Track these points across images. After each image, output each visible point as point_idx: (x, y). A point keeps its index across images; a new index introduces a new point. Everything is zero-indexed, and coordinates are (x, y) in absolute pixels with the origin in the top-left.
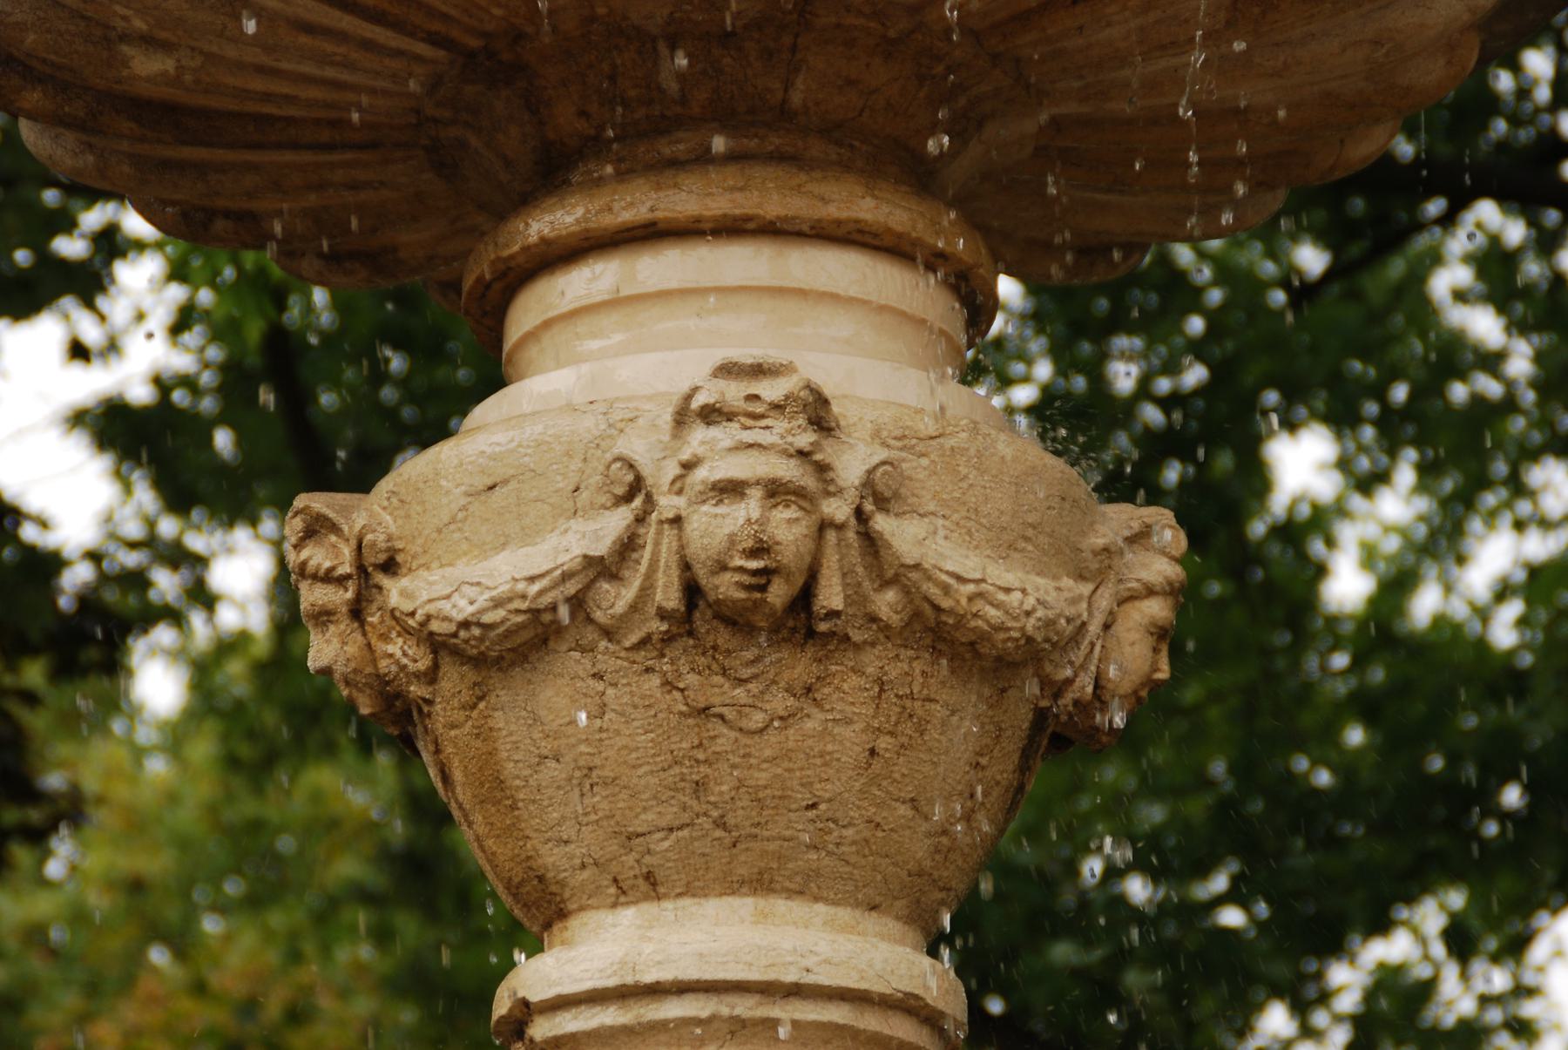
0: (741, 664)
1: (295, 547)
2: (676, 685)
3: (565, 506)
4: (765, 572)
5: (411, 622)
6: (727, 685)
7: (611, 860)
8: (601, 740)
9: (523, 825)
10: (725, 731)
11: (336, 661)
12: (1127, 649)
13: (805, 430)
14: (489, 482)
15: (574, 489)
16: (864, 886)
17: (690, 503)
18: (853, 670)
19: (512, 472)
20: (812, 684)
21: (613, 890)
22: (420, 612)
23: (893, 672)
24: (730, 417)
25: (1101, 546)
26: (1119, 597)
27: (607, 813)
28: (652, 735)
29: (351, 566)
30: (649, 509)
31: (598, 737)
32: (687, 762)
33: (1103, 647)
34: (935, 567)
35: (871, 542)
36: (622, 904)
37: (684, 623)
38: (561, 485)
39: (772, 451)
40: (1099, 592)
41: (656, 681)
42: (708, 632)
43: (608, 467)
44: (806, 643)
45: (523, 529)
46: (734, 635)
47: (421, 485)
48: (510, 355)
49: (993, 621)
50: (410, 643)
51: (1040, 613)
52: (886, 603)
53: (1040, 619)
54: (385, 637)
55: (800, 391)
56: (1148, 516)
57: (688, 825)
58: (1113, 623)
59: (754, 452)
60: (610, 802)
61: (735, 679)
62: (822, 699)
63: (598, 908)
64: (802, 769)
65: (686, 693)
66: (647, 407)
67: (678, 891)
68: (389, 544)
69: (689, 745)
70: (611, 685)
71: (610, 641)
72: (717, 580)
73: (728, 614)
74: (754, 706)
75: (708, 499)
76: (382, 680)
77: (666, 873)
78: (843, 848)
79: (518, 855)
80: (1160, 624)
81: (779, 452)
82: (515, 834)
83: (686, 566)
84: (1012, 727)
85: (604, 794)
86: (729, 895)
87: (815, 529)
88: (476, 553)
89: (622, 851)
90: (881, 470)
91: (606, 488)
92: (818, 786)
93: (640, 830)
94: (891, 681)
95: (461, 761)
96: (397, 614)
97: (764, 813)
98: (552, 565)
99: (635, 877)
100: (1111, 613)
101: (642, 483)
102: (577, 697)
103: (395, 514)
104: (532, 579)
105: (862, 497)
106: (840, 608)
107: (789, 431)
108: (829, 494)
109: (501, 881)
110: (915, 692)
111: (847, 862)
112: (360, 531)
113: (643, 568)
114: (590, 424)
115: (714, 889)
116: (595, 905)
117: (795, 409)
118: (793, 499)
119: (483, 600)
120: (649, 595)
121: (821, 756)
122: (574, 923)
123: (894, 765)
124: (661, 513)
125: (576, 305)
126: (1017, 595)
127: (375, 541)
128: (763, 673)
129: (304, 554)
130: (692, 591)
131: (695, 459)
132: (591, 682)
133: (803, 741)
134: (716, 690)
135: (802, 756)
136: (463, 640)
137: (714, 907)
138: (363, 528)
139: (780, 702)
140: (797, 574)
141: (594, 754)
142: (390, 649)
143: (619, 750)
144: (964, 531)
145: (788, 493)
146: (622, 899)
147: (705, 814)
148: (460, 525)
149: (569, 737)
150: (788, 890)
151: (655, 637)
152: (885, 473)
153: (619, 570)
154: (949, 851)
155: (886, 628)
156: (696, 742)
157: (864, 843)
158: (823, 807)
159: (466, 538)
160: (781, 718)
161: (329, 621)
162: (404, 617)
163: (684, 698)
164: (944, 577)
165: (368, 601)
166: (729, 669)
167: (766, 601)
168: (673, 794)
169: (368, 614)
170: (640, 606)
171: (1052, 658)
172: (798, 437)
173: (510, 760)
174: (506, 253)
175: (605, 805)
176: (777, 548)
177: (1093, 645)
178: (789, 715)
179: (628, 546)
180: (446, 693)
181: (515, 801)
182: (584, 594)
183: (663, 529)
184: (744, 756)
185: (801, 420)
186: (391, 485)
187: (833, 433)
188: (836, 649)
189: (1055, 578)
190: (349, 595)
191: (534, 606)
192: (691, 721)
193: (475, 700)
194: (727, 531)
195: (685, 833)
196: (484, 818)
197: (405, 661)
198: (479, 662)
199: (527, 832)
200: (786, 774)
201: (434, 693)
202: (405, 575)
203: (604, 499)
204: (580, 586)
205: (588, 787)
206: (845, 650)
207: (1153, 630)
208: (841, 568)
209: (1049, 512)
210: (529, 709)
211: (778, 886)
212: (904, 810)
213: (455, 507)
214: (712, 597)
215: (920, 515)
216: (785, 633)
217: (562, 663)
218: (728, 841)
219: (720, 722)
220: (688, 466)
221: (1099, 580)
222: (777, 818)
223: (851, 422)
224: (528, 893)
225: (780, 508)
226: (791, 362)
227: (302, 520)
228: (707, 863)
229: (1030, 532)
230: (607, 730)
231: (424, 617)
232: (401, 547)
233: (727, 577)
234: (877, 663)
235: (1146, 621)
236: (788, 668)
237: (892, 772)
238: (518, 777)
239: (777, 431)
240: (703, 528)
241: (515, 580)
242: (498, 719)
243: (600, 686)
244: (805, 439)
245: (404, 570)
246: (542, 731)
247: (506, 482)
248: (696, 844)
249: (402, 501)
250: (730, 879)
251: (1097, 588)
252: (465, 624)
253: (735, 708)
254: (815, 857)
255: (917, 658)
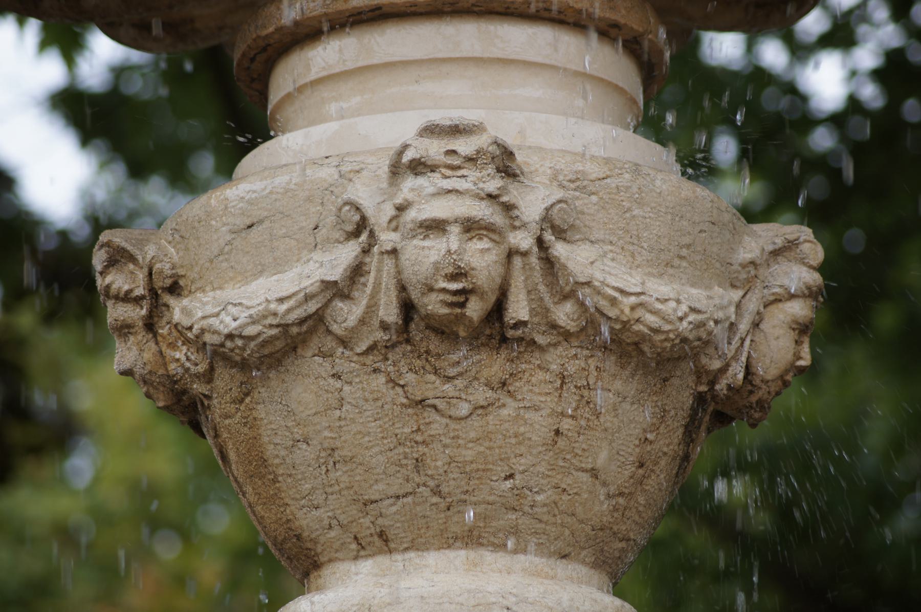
0: (449, 365)
1: (101, 273)
2: (398, 382)
3: (308, 241)
4: (464, 292)
5: (189, 335)
6: (438, 382)
7: (352, 522)
8: (340, 427)
9: (283, 494)
10: (438, 418)
11: (136, 365)
12: (773, 343)
13: (493, 178)
14: (248, 223)
15: (314, 227)
16: (555, 539)
17: (404, 238)
18: (539, 366)
19: (266, 214)
20: (506, 379)
21: (354, 546)
22: (196, 327)
23: (572, 368)
24: (433, 168)
25: (748, 260)
26: (764, 300)
27: (348, 484)
28: (381, 422)
29: (144, 289)
30: (373, 243)
31: (338, 424)
32: (408, 443)
33: (752, 341)
34: (602, 283)
35: (549, 263)
36: (362, 557)
37: (403, 333)
38: (304, 224)
39: (467, 196)
40: (748, 296)
41: (382, 379)
42: (422, 340)
43: (340, 210)
44: (500, 347)
45: (275, 259)
46: (443, 341)
47: (196, 224)
48: (272, 113)
49: (652, 326)
50: (192, 350)
51: (692, 317)
52: (564, 315)
53: (690, 323)
54: (173, 346)
55: (488, 148)
56: (792, 233)
57: (411, 493)
58: (760, 321)
59: (453, 197)
60: (349, 476)
61: (444, 376)
62: (514, 391)
63: (343, 560)
64: (501, 447)
65: (406, 388)
66: (370, 161)
67: (405, 545)
68: (174, 271)
69: (409, 430)
70: (347, 383)
71: (345, 348)
72: (426, 300)
73: (436, 325)
74: (460, 398)
75: (417, 235)
76: (172, 380)
77: (396, 532)
78: (536, 509)
79: (280, 519)
80: (801, 321)
81: (472, 196)
82: (277, 502)
83: (402, 288)
84: (674, 408)
85: (344, 469)
86: (445, 549)
87: (504, 255)
88: (240, 279)
89: (361, 515)
90: (560, 205)
91: (338, 227)
92: (514, 460)
93: (373, 498)
94: (571, 375)
95: (234, 445)
96: (180, 328)
97: (471, 483)
98: (297, 288)
99: (371, 535)
100: (758, 313)
101: (367, 222)
102: (321, 393)
103: (178, 247)
104: (281, 300)
105: (542, 229)
106: (526, 319)
107: (480, 179)
108: (515, 228)
109: (269, 538)
110: (590, 383)
111: (540, 521)
112: (150, 261)
113: (369, 290)
114: (327, 173)
115: (433, 544)
116: (341, 558)
117: (485, 161)
118: (485, 233)
119: (242, 320)
120: (374, 311)
121: (516, 437)
122: (326, 571)
123: (575, 442)
124: (381, 246)
125: (324, 73)
126: (673, 304)
127: (162, 269)
128: (466, 371)
129: (108, 279)
130: (408, 308)
131: (406, 203)
132: (331, 381)
133: (501, 425)
134: (430, 386)
135: (500, 437)
136: (229, 349)
137: (433, 558)
138: (153, 258)
139: (481, 395)
140: (490, 293)
141: (335, 438)
142: (178, 355)
143: (354, 434)
144: (627, 254)
145: (480, 229)
146: (362, 553)
147: (425, 485)
148: (227, 256)
149: (315, 424)
150: (493, 544)
151: (379, 345)
152: (561, 210)
153: (350, 291)
154: (625, 509)
155: (567, 335)
156: (415, 428)
157: (553, 505)
158: (518, 477)
159: (232, 267)
160: (482, 407)
161: (129, 333)
162: (184, 331)
163: (405, 392)
164: (610, 292)
165: (159, 316)
166: (439, 369)
167: (465, 315)
168: (398, 469)
169: (159, 327)
170: (367, 320)
171: (707, 352)
172: (488, 183)
173: (270, 443)
174: (265, 32)
175: (345, 478)
176: (472, 272)
177: (743, 340)
178: (489, 405)
179: (357, 271)
180: (221, 390)
181: (276, 476)
182: (323, 311)
183: (383, 259)
184: (453, 438)
185: (491, 170)
186: (174, 225)
187: (517, 178)
188: (525, 351)
189: (708, 287)
190: (144, 312)
191: (283, 322)
192: (410, 411)
193: (243, 396)
194: (432, 259)
195: (409, 499)
196: (254, 489)
197: (188, 364)
198: (244, 366)
199: (287, 500)
200: (488, 452)
201: (211, 390)
202: (188, 296)
203: (337, 235)
204: (320, 305)
205: (332, 463)
206: (532, 352)
207: (794, 326)
208: (526, 286)
209: (701, 235)
210: (284, 403)
211: (485, 541)
212: (585, 477)
213: (222, 242)
214: (423, 311)
215: (592, 242)
216: (483, 339)
217: (309, 366)
218: (443, 506)
219: (434, 411)
220: (401, 209)
221: (747, 288)
222: (481, 486)
223: (533, 169)
224: (290, 548)
225: (475, 240)
226: (481, 123)
227: (106, 252)
228: (427, 523)
229: (684, 252)
230: (345, 419)
231: (199, 331)
232: (183, 273)
233: (434, 296)
234: (559, 361)
235: (789, 319)
236: (486, 367)
237: (574, 448)
238: (277, 456)
239: (471, 178)
240: (413, 258)
241: (267, 301)
242: (261, 412)
243: (338, 384)
244: (493, 185)
245: (186, 292)
246: (295, 420)
247: (261, 222)
248: (418, 509)
249: (182, 237)
250: (446, 536)
251: (746, 294)
252: (230, 336)
253: (445, 399)
254: (514, 517)
255: (592, 356)
